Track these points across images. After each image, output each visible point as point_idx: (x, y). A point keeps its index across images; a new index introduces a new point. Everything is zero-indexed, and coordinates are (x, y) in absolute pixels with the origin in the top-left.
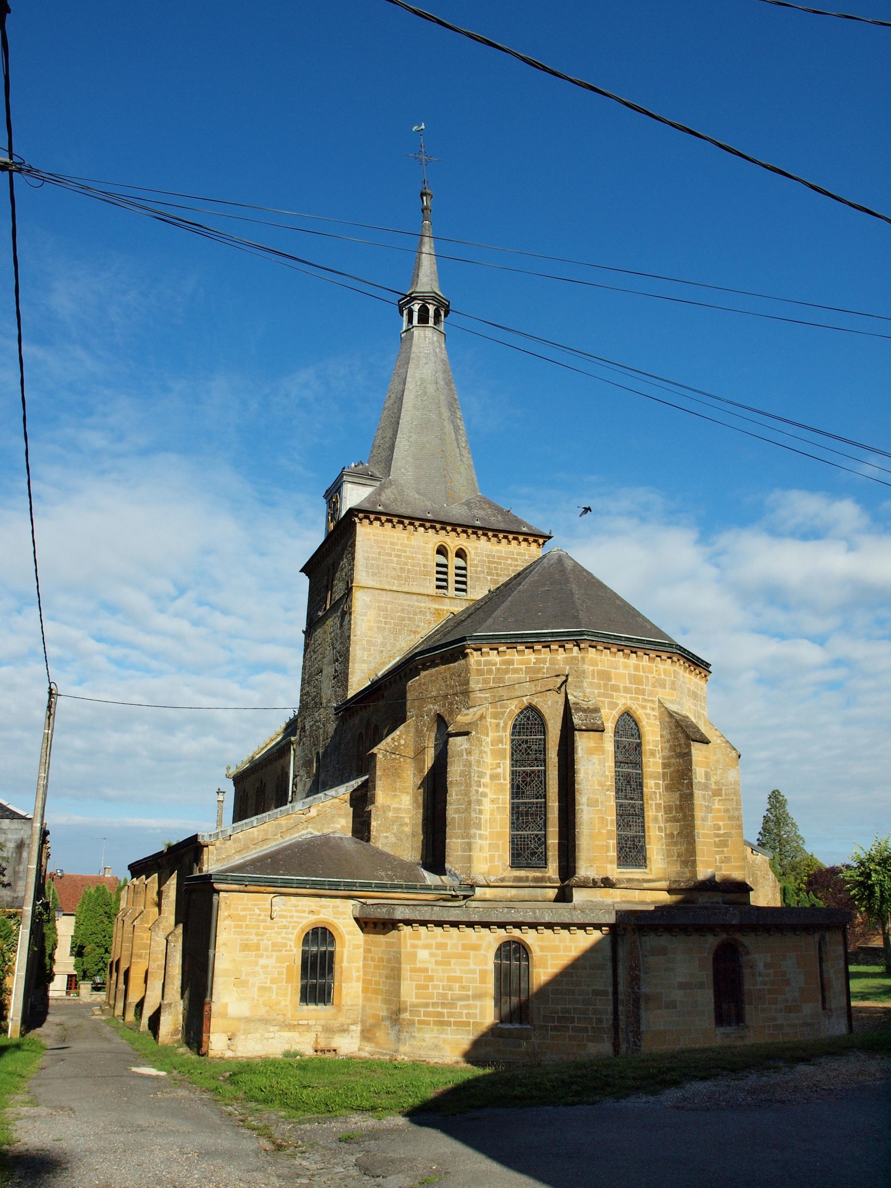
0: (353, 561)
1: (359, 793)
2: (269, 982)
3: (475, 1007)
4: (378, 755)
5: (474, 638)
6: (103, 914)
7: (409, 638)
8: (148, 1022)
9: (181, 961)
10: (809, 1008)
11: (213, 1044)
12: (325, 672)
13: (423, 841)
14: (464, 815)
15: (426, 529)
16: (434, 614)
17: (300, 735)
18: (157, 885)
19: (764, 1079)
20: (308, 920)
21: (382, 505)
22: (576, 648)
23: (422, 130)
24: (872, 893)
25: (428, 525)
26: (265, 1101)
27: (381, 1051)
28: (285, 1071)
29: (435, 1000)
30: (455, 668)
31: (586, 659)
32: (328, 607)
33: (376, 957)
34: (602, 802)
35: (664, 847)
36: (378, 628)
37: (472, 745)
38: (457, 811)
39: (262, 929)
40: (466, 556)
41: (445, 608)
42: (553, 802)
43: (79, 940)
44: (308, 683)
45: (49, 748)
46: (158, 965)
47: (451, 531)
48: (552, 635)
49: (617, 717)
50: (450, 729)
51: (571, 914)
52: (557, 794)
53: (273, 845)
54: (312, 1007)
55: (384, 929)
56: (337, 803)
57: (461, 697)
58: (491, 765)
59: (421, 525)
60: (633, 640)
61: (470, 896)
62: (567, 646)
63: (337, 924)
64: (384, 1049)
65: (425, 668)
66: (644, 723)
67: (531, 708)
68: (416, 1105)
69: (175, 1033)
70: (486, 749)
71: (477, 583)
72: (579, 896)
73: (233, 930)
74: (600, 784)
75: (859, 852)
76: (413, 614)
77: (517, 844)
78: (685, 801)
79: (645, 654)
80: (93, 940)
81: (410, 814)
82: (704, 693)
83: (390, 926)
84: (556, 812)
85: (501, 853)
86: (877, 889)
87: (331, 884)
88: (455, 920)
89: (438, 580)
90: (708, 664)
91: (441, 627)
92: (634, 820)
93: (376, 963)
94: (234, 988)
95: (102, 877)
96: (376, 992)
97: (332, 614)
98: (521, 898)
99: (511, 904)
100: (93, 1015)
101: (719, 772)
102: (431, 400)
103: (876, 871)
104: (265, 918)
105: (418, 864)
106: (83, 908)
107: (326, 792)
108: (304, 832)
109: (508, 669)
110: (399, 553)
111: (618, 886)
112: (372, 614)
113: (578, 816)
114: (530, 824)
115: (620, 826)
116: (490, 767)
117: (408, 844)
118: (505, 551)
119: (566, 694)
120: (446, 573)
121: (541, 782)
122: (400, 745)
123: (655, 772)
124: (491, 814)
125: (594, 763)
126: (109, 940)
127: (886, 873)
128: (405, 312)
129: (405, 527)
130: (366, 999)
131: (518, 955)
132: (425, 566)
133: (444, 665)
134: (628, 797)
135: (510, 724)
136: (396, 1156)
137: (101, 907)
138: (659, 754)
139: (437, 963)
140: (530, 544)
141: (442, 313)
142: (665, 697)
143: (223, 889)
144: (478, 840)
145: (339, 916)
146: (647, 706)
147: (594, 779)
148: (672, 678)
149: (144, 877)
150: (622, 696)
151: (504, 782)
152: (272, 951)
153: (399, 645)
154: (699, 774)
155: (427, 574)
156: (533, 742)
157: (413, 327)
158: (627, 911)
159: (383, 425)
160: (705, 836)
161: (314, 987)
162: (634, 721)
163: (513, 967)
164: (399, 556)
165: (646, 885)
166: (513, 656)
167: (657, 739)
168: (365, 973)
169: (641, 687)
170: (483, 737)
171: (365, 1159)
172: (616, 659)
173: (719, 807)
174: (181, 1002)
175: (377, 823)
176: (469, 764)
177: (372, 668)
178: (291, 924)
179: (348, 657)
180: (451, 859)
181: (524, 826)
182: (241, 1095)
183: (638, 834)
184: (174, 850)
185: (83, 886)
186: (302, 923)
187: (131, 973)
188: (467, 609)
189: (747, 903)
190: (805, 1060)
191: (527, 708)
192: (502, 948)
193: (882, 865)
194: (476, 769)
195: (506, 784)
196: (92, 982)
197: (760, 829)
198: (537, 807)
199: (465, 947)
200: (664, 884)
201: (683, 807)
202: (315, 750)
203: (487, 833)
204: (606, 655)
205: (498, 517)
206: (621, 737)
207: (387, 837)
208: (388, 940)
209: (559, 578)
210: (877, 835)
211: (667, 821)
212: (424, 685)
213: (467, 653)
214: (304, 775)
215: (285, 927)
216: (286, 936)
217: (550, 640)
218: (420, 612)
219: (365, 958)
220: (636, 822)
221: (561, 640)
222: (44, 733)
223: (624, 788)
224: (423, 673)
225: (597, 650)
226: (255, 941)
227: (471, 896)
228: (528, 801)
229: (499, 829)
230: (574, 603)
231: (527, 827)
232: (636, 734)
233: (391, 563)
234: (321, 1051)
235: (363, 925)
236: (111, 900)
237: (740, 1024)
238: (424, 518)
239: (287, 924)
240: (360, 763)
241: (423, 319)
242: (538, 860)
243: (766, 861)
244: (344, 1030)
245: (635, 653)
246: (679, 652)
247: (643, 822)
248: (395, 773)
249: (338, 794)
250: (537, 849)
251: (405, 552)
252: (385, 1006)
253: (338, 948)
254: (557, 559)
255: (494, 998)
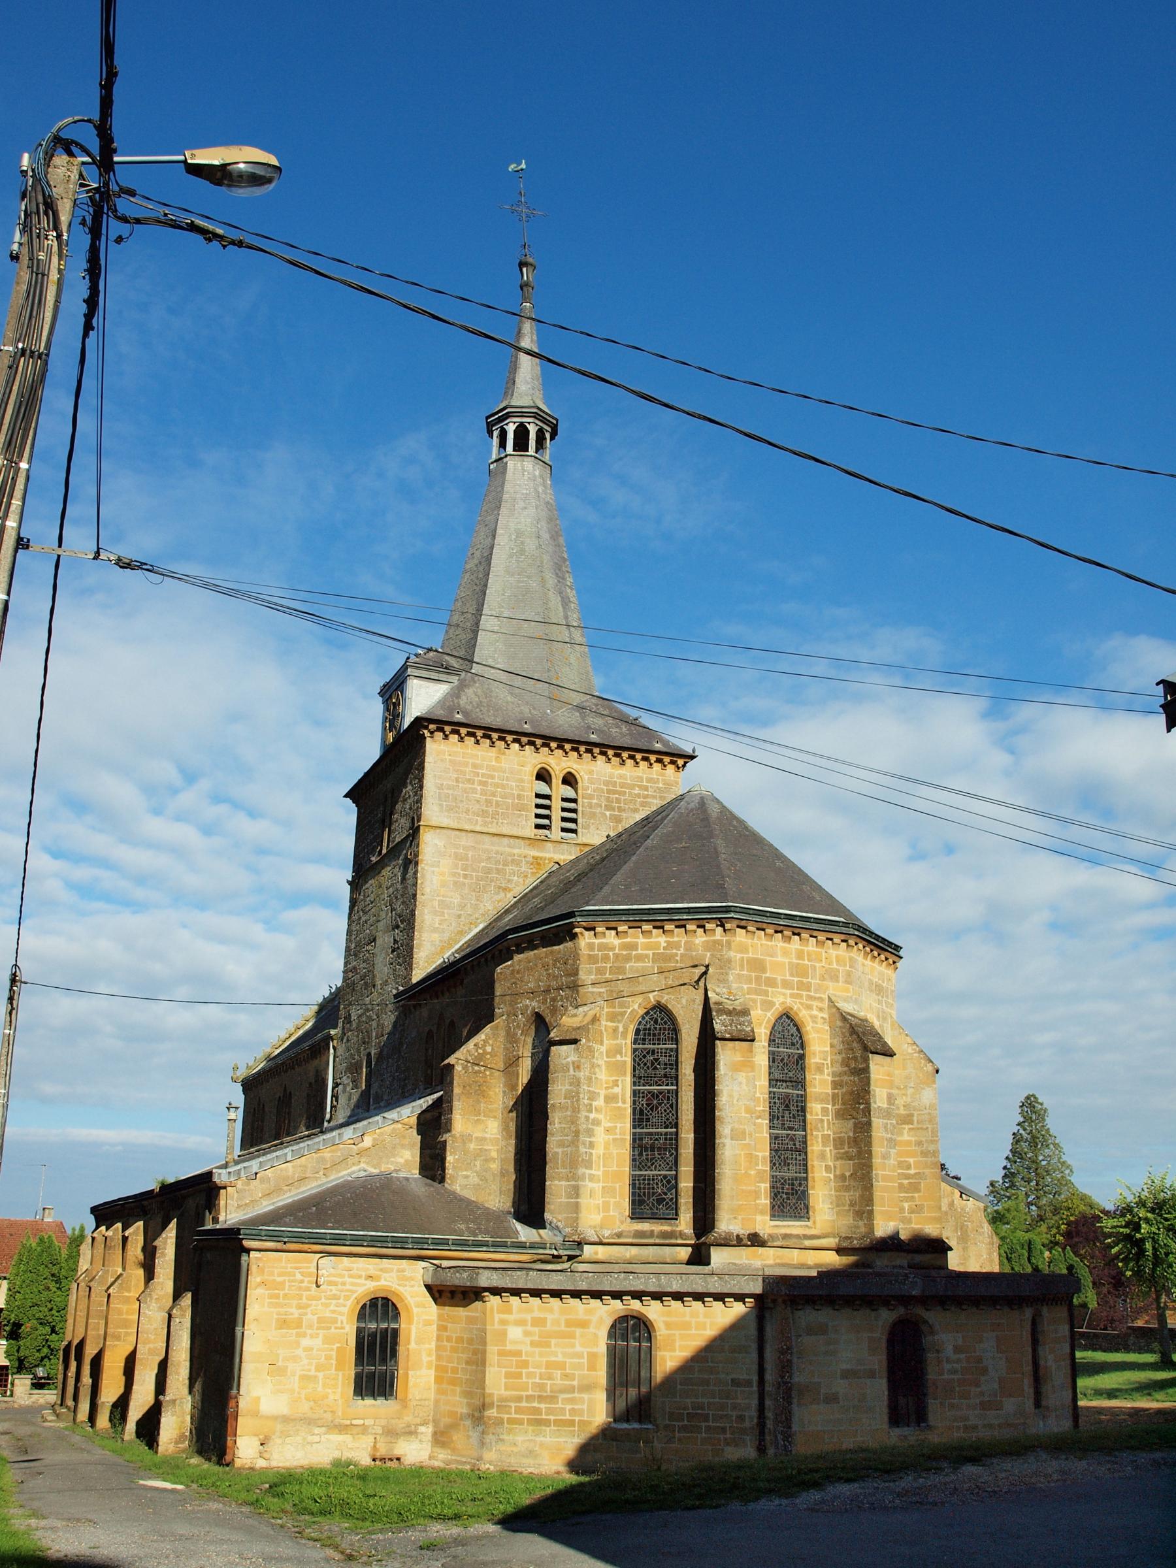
0: (421, 790)
1: (428, 1116)
2: (313, 1368)
3: (582, 1400)
4: (456, 1067)
5: (585, 913)
6: (49, 1276)
7: (497, 897)
8: (135, 1427)
9: (189, 1342)
10: (1013, 1406)
11: (240, 1451)
12: (379, 942)
13: (515, 1182)
14: (569, 1149)
15: (522, 746)
16: (532, 864)
17: (343, 1028)
18: (142, 1238)
19: (921, 1480)
20: (365, 1287)
21: (462, 712)
22: (720, 929)
23: (522, 170)
24: (1142, 1252)
25: (524, 740)
26: (323, 1513)
27: (459, 1458)
28: (340, 1480)
29: (530, 1393)
30: (559, 952)
31: (733, 944)
32: (384, 851)
33: (454, 1336)
34: (751, 1135)
35: (833, 1192)
36: (455, 883)
37: (580, 1056)
38: (561, 1144)
39: (304, 1300)
40: (577, 783)
41: (548, 855)
42: (688, 1132)
43: (13, 1315)
44: (356, 955)
45: (10, 1054)
46: (149, 1349)
47: (556, 748)
48: (689, 911)
49: (773, 1020)
50: (552, 1035)
51: (706, 1282)
52: (692, 1122)
53: (313, 1185)
54: (369, 1402)
55: (464, 1299)
56: (399, 1129)
57: (568, 992)
58: (606, 1083)
59: (515, 741)
60: (795, 918)
61: (578, 1256)
62: (708, 926)
63: (403, 1294)
64: (463, 1456)
65: (520, 951)
66: (808, 1028)
67: (660, 1008)
68: (509, 1513)
69: (180, 1439)
70: (600, 1062)
71: (592, 821)
72: (719, 1257)
73: (267, 1300)
74: (749, 1110)
75: (1126, 1193)
76: (503, 865)
77: (639, 1188)
78: (860, 1132)
79: (811, 936)
80: (34, 1315)
81: (498, 1145)
82: (891, 986)
83: (472, 1295)
84: (691, 1146)
85: (618, 1200)
86: (1148, 1246)
87: (395, 1240)
88: (556, 1288)
89: (537, 816)
90: (898, 947)
91: (541, 882)
92: (794, 1156)
93: (454, 1344)
94: (268, 1378)
95: (40, 1222)
96: (453, 1382)
97: (390, 861)
98: (644, 1259)
99: (630, 1268)
100: (44, 1422)
101: (910, 1091)
102: (530, 561)
103: (1147, 1220)
104: (309, 1285)
105: (509, 1213)
106: (19, 1268)
107: (386, 1115)
108: (355, 1168)
109: (630, 955)
110: (484, 779)
111: (769, 1244)
112: (446, 865)
113: (719, 1152)
114: (656, 1161)
115: (774, 1164)
116: (605, 1086)
117: (495, 1187)
118: (631, 776)
119: (706, 990)
120: (548, 807)
121: (671, 1106)
122: (485, 1053)
123: (822, 1093)
124: (606, 1148)
125: (740, 1083)
126: (57, 1314)
127: (1161, 1223)
128: (496, 434)
129: (493, 743)
130: (440, 1392)
131: (637, 1334)
132: (519, 797)
133: (546, 947)
134: (786, 1126)
135: (632, 1029)
136: (489, 1558)
137: (46, 1266)
138: (828, 1069)
139: (532, 1344)
140: (665, 766)
141: (548, 436)
142: (838, 993)
143: (255, 1247)
144: (587, 1182)
145: (405, 1283)
146: (813, 1005)
147: (741, 1103)
148: (848, 968)
149: (119, 1225)
150: (780, 993)
151: (623, 1106)
152: (318, 1329)
153: (483, 907)
154: (879, 1097)
155: (522, 808)
156: (661, 1053)
157: (506, 456)
158: (782, 1277)
159: (463, 594)
160: (887, 1178)
161: (372, 1375)
162: (795, 1025)
163: (631, 1350)
164: (484, 784)
165: (807, 1243)
166: (637, 938)
167: (826, 1049)
168: (439, 1358)
169: (805, 980)
170: (596, 1046)
171: (453, 1563)
172: (773, 943)
173: (909, 1138)
174: (189, 1398)
175: (454, 1159)
176: (577, 1082)
177: (446, 938)
178: (343, 1294)
179: (413, 924)
180: (552, 1207)
181: (649, 1164)
182: (288, 1507)
183: (798, 1175)
184: (169, 1190)
185: (11, 1235)
186: (357, 1291)
187: (105, 1360)
188: (577, 859)
189: (945, 1266)
190: (973, 1460)
191: (653, 1008)
192: (618, 1325)
193: (1157, 1211)
194: (586, 1088)
195: (625, 1109)
196: (31, 1376)
197: (1008, 1153)
198: (666, 1139)
199: (569, 1323)
200: (832, 1242)
201: (858, 1139)
202: (365, 1049)
203: (600, 1173)
204: (759, 938)
205: (621, 729)
206: (778, 1047)
207: (467, 1177)
208: (470, 1314)
209: (700, 830)
210: (1150, 1169)
211: (837, 1159)
212: (518, 972)
213: (576, 933)
214: (348, 1084)
215: (335, 1297)
216: (336, 1309)
217: (685, 917)
218: (513, 861)
219: (439, 1338)
220: (796, 1159)
221: (701, 918)
222: (4, 1034)
223: (780, 1115)
224: (517, 957)
225: (747, 931)
226: (296, 1316)
227: (578, 1256)
228: (654, 1130)
229: (615, 1168)
230: (718, 866)
231: (652, 1165)
232: (797, 1042)
233: (473, 793)
234: (381, 1460)
235: (437, 1295)
236: (60, 1256)
237: (922, 1425)
238: (520, 730)
239: (338, 1293)
240: (429, 1072)
241: (521, 443)
242: (667, 1209)
243: (979, 1209)
244: (410, 1432)
245: (799, 934)
246: (857, 933)
247: (805, 1160)
248: (479, 1091)
249: (401, 1117)
250: (666, 1194)
251: (493, 777)
252: (465, 1401)
253: (403, 1325)
254: (698, 803)
255: (606, 1389)
